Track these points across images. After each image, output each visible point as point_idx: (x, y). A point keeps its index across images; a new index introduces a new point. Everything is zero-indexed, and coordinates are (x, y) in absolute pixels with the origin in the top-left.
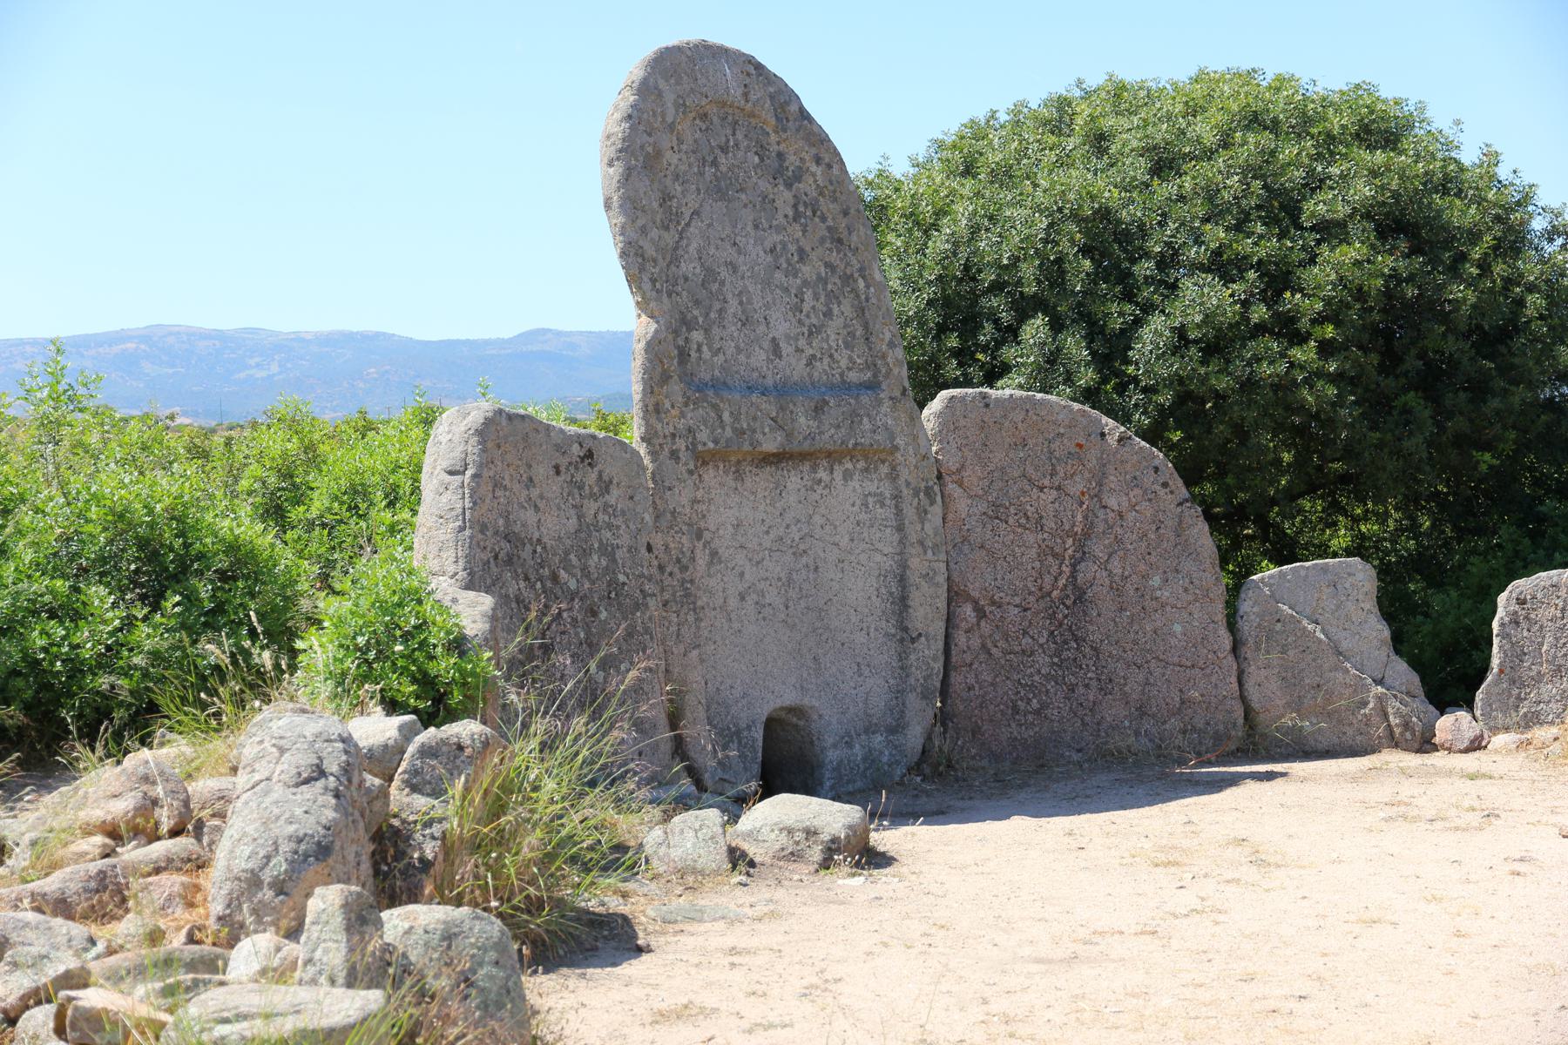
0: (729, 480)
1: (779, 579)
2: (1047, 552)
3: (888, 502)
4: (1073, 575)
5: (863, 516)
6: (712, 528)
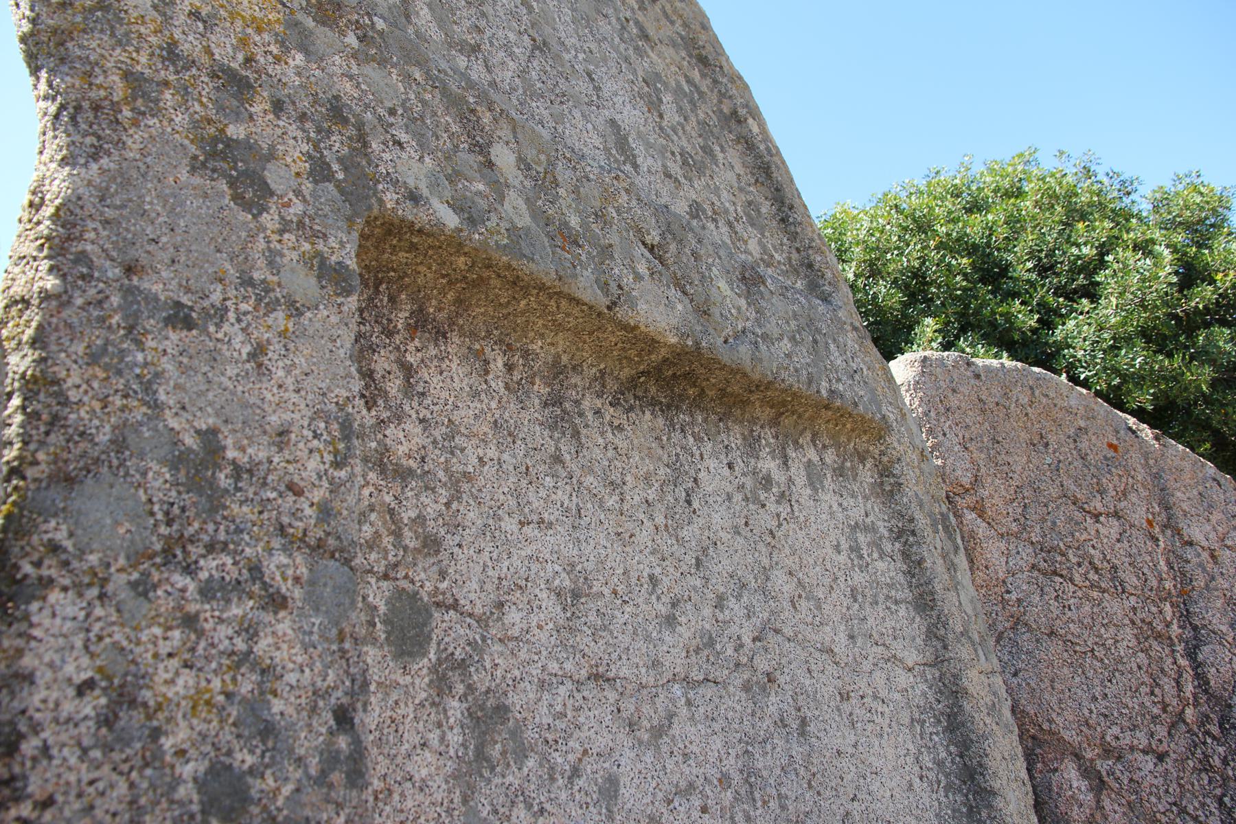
0: (530, 419)
1: (725, 780)
2: (1148, 633)
3: (888, 547)
4: (1201, 678)
5: (859, 578)
6: (473, 596)
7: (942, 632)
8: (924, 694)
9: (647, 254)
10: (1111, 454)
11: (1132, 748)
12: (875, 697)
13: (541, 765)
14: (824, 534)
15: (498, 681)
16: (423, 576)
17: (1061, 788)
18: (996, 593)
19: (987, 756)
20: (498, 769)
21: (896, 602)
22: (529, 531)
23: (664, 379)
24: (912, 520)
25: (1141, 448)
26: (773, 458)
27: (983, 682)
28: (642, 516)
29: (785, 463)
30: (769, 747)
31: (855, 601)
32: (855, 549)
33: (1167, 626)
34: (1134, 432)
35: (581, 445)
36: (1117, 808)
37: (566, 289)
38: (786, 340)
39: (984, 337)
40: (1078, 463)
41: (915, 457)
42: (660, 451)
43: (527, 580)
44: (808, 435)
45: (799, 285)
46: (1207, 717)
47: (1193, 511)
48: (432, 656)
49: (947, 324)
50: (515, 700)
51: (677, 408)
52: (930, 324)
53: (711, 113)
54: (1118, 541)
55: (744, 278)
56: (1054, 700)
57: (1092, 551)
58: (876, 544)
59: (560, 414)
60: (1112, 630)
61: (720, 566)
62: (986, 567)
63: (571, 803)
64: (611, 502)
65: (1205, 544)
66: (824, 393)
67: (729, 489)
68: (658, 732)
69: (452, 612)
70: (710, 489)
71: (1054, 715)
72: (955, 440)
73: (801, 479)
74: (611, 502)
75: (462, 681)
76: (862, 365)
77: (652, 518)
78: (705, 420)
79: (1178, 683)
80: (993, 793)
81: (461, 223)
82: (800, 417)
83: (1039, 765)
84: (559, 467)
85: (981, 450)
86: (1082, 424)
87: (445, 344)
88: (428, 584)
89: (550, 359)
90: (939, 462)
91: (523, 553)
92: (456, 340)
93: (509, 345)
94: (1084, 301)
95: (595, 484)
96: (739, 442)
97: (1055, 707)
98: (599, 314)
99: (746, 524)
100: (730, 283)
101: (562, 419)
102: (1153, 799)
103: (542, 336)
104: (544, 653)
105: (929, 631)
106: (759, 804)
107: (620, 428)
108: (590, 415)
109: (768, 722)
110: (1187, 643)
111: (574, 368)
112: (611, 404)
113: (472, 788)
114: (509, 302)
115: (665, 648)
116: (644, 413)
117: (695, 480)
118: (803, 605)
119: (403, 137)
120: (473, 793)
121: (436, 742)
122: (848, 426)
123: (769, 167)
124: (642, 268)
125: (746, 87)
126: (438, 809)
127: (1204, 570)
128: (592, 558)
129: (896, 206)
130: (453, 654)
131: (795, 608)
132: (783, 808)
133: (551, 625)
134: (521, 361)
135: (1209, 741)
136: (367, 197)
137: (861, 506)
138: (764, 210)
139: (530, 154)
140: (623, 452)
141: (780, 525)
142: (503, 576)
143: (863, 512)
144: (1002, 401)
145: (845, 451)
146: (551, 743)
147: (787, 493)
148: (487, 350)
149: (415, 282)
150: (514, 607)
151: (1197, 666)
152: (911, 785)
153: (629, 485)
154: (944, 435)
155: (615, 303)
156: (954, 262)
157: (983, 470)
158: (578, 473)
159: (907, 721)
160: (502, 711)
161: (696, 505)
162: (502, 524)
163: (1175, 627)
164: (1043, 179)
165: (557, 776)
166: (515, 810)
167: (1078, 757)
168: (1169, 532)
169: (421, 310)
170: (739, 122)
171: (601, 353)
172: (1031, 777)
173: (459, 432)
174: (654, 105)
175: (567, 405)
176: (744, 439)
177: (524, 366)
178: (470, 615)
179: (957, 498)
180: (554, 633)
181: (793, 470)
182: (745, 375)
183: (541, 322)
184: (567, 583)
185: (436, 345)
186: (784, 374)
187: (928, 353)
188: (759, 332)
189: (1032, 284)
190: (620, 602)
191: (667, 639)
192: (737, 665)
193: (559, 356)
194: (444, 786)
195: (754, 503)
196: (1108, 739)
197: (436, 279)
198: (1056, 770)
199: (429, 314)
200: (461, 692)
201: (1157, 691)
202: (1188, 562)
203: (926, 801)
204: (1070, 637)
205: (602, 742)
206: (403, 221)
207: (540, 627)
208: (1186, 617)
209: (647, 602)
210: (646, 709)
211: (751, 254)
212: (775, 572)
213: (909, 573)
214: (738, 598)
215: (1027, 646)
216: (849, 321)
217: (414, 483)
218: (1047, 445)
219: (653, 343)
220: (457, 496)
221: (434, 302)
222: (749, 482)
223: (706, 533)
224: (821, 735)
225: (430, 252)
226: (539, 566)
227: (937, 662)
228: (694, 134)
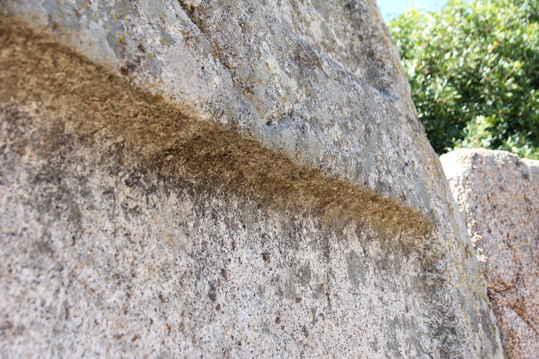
3: (426, 343)
9: (184, 15)
14: (362, 330)
23: (196, 159)
24: (452, 318)
26: (314, 249)
28: (151, 314)
29: (326, 255)
35: (81, 230)
37: (63, 41)
38: (336, 127)
39: (531, 138)
41: (459, 253)
42: (184, 239)
44: (353, 226)
45: (358, 73)
49: (497, 123)
51: (210, 191)
52: (482, 123)
55: (298, 58)
58: (415, 341)
59: (56, 192)
66: (372, 185)
67: (262, 281)
70: (239, 282)
72: (500, 238)
73: (341, 273)
76: (414, 158)
77: (164, 315)
78: (242, 206)
82: (345, 207)
89: (49, 126)
90: (483, 258)
95: (95, 276)
96: (277, 231)
98: (111, 77)
99: (278, 320)
100: (281, 61)
101: (59, 198)
103: (38, 97)
107: (136, 211)
108: (98, 196)
112: (127, 183)
116: (168, 195)
117: (223, 272)
122: (395, 219)
124: (174, 31)
137: (403, 301)
140: (137, 239)
141: (315, 321)
143: (404, 308)
145: (390, 244)
147: (326, 287)
153: (140, 277)
154: (489, 231)
155: (132, 67)
157: (525, 269)
158: (72, 263)
161: (220, 299)
171: (118, 124)
175: (68, 182)
176: (284, 227)
179: (498, 296)
181: (333, 261)
182: (287, 161)
183: (33, 80)
186: (331, 163)
187: (479, 151)
188: (308, 116)
193: (62, 124)
195: (288, 297)
211: (312, 36)
216: (404, 113)
219: (180, 119)
222: (285, 274)
223: (230, 333)
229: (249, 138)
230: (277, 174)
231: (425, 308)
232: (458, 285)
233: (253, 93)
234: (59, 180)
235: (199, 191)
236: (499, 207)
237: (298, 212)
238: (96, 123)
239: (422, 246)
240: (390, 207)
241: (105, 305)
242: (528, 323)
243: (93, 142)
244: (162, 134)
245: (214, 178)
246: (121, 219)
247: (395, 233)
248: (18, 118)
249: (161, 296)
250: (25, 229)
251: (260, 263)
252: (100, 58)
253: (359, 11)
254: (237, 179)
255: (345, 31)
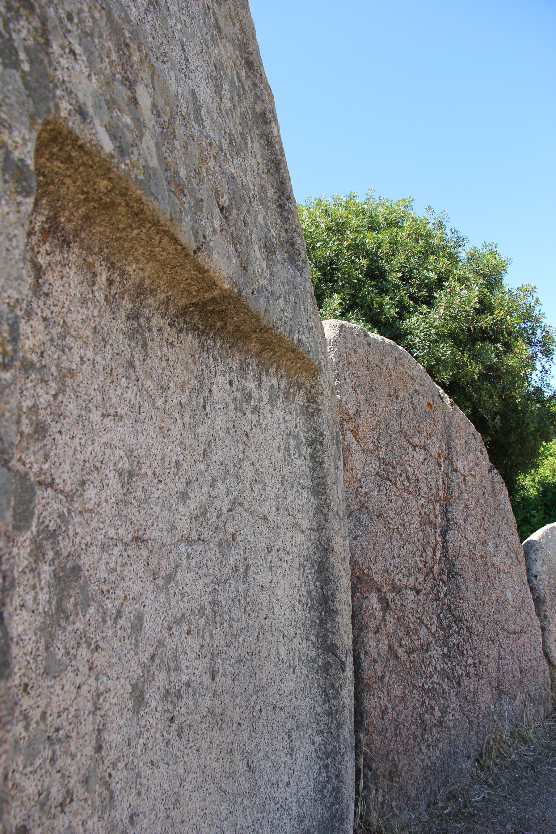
3: (304, 450)
4: (445, 548)
6: (66, 477)
7: (326, 510)
8: (308, 548)
10: (428, 409)
11: (406, 587)
12: (285, 550)
13: (98, 611)
15: (76, 546)
16: (32, 458)
17: (367, 608)
18: (354, 486)
19: (337, 590)
20: (71, 619)
21: (303, 488)
22: (108, 422)
24: (322, 435)
25: (443, 409)
27: (341, 545)
28: (176, 415)
29: (260, 385)
30: (227, 585)
31: (283, 485)
32: (287, 450)
33: (436, 517)
34: (442, 398)
35: (146, 355)
36: (392, 620)
37: (172, 230)
39: (364, 315)
40: (411, 412)
42: (193, 366)
43: (102, 462)
44: (275, 366)
46: (443, 570)
47: (461, 452)
48: (34, 529)
50: (85, 561)
51: (208, 334)
53: (248, 109)
54: (422, 463)
56: (373, 556)
57: (409, 468)
58: (298, 447)
60: (410, 517)
61: (218, 456)
62: (352, 470)
63: (115, 638)
64: (160, 402)
65: (462, 472)
68: (169, 578)
69: (49, 490)
71: (371, 565)
72: (351, 384)
74: (160, 402)
75: (53, 549)
77: (182, 417)
78: (221, 347)
79: (434, 550)
80: (337, 612)
81: (114, 150)
83: (358, 594)
84: (131, 371)
85: (363, 393)
86: (417, 387)
87: (68, 251)
88: (35, 466)
89: (138, 281)
91: (102, 441)
92: (76, 250)
93: (112, 263)
94: (425, 306)
95: (152, 387)
96: (238, 366)
97: (373, 561)
99: (234, 427)
102: (410, 616)
103: (138, 261)
104: (108, 522)
105: (318, 508)
106: (218, 625)
107: (171, 344)
108: (155, 330)
109: (229, 567)
110: (442, 528)
111: (151, 291)
113: (52, 636)
114: (125, 229)
115: (179, 517)
116: (188, 335)
118: (257, 486)
119: (78, 49)
120: (53, 640)
121: (31, 602)
122: (299, 365)
123: (279, 164)
125: (273, 97)
126: (28, 658)
127: (459, 487)
128: (144, 446)
129: (326, 210)
130: (48, 526)
131: (252, 488)
132: (231, 626)
133: (113, 499)
134: (118, 279)
135: (441, 584)
136: (47, 99)
137: (295, 422)
138: (269, 195)
139: (161, 103)
141: (252, 429)
142: (87, 459)
144: (379, 364)
146: (105, 592)
148: (97, 264)
149: (58, 191)
150: (92, 485)
151: (445, 541)
152: (294, 607)
154: (345, 379)
156: (357, 260)
159: (297, 566)
160: (77, 569)
161: (208, 410)
162: (91, 415)
163: (439, 518)
164: (416, 221)
165: (108, 618)
166: (80, 649)
167: (379, 590)
168: (447, 462)
169: (55, 217)
170: (265, 122)
171: (172, 283)
172: (353, 601)
173: (69, 333)
174: (218, 89)
175: (142, 320)
176: (241, 364)
177: (120, 283)
178: (62, 492)
180: (115, 505)
181: (263, 390)
182: (258, 320)
183: (142, 250)
184: (127, 465)
185: (61, 252)
189: (398, 287)
190: (156, 481)
191: (181, 509)
192: (217, 528)
193: (144, 280)
194: (34, 638)
196: (396, 581)
197: (76, 194)
198: (366, 598)
199: (60, 222)
200: (51, 557)
201: (424, 555)
202: (453, 481)
203: (300, 616)
204: (388, 519)
205: (136, 588)
206: (70, 132)
207: (106, 501)
208: (445, 512)
209: (173, 481)
210: (164, 562)
212: (245, 463)
213: (313, 469)
214: (224, 480)
215: (365, 522)
217: (33, 376)
218: (397, 397)
219: (213, 284)
220: (61, 390)
221: (67, 213)
222: (239, 395)
224: (255, 576)
225: (82, 169)
226: (111, 451)
227: (319, 529)
228: (238, 123)
229: (245, 303)
230: (247, 328)
231: (306, 427)
232: (327, 414)
233: (247, 271)
234: (138, 318)
235: (201, 333)
236: (352, 364)
237: (249, 354)
238: (161, 282)
239: (309, 385)
240: (300, 357)
241: (156, 407)
242: (358, 442)
243: (156, 294)
244: (194, 293)
245: (211, 325)
246: (165, 349)
247: (295, 374)
248: (124, 275)
249: (181, 404)
250: (123, 351)
251: (228, 387)
252: (188, 242)
253: (288, 211)
254: (222, 327)
255: (276, 224)
